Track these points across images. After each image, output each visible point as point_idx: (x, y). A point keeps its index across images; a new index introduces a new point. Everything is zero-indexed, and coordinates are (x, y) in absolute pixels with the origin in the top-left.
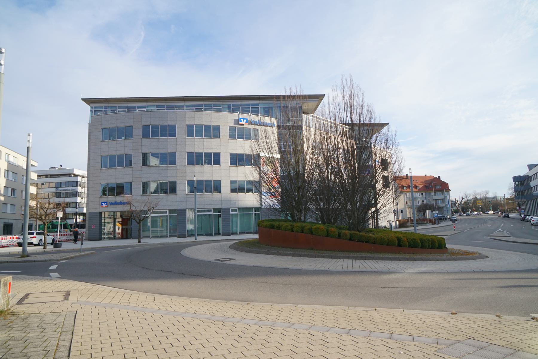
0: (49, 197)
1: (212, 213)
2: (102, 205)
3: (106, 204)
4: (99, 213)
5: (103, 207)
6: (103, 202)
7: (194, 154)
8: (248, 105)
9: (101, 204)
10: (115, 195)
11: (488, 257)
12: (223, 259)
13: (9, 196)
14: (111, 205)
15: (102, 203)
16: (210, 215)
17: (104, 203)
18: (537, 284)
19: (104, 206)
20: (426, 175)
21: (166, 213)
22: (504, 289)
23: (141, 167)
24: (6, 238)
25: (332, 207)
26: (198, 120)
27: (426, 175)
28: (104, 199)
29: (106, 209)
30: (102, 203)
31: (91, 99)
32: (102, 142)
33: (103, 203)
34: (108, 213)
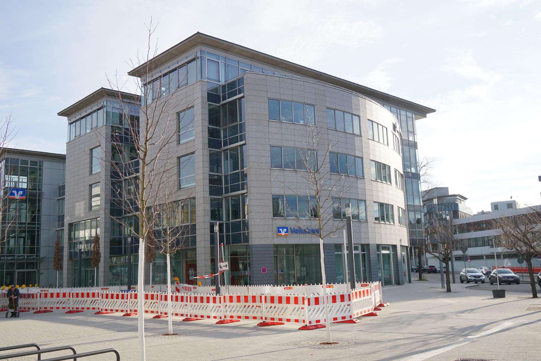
2: (280, 232)
3: (285, 230)
4: (272, 246)
5: (281, 235)
7: (296, 167)
9: (275, 229)
11: (466, 288)
12: (132, 338)
13: (93, 190)
14: (292, 232)
17: (283, 228)
18: (121, 360)
19: (283, 233)
21: (17, 256)
22: (487, 322)
24: (125, 297)
25: (126, 257)
28: (280, 222)
29: (285, 239)
30: (279, 228)
32: (270, 122)
33: (281, 230)
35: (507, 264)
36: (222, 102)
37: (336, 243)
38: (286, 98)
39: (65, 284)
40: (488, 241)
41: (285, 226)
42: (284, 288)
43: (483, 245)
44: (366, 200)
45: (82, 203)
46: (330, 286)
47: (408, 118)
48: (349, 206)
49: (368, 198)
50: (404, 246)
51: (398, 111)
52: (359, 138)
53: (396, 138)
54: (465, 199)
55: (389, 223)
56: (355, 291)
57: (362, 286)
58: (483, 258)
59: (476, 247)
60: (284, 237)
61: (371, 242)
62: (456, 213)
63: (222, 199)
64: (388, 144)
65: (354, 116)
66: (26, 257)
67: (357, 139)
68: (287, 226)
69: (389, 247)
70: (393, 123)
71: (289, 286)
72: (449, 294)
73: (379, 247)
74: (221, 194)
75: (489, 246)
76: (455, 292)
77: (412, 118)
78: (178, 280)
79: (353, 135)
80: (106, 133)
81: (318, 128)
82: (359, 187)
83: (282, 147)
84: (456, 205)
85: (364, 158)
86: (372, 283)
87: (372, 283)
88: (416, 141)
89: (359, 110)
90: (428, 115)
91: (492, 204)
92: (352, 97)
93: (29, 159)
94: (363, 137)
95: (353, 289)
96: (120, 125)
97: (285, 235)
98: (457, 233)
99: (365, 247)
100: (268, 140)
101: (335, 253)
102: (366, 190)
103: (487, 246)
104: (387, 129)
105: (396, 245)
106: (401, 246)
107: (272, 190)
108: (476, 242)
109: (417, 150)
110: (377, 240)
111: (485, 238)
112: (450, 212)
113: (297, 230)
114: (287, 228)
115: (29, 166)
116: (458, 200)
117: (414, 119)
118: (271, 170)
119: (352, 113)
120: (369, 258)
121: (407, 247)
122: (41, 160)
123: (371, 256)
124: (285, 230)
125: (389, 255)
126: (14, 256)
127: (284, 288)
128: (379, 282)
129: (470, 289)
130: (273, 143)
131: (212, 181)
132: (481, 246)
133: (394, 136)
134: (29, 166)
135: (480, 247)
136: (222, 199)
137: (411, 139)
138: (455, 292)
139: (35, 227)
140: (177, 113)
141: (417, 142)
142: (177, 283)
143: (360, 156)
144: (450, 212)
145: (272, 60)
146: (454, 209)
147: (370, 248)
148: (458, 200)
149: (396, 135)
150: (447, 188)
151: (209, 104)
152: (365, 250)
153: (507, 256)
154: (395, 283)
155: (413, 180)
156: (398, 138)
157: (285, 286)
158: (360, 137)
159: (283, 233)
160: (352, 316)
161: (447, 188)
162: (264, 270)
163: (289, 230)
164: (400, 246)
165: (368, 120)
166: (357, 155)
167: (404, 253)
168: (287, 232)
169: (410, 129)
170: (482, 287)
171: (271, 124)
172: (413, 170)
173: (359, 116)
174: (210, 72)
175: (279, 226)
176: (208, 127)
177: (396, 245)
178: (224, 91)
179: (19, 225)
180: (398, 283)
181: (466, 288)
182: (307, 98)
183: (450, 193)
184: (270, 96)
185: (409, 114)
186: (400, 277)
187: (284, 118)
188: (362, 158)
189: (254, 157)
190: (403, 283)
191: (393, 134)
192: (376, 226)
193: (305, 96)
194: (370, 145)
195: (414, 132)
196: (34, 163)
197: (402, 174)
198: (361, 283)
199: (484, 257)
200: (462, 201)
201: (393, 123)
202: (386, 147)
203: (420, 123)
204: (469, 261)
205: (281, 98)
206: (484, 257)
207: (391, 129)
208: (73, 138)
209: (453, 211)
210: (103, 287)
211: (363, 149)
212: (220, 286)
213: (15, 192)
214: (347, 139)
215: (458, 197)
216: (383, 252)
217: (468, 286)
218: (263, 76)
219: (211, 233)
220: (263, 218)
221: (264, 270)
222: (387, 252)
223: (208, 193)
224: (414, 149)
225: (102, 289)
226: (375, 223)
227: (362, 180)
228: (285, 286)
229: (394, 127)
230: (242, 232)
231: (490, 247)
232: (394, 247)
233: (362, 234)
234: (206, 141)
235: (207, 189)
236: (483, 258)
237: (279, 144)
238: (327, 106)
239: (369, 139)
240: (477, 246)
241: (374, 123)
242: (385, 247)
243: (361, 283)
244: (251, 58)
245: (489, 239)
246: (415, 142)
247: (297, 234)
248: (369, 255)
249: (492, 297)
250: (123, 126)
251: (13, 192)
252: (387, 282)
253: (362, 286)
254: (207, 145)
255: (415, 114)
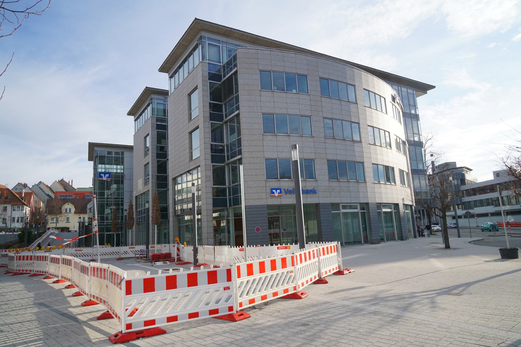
0: (2, 4)
1: (358, 210)
2: (274, 193)
3: (279, 191)
6: (274, 189)
8: (136, 211)
9: (269, 191)
10: (277, 178)
11: (469, 242)
15: (272, 189)
16: (364, 212)
17: (276, 190)
19: (276, 194)
20: (33, 186)
23: (324, 139)
26: (230, 165)
27: (33, 186)
28: (274, 183)
29: (279, 200)
30: (272, 189)
31: (216, 26)
34: (451, 239)
35: (510, 219)
36: (223, 79)
37: (333, 202)
38: (277, 69)
39: (134, 243)
40: (492, 202)
41: (279, 188)
42: (240, 249)
43: (488, 205)
44: (364, 162)
45: (141, 180)
46: (286, 247)
47: (409, 94)
48: (296, 148)
49: (365, 160)
50: (408, 205)
51: (399, 88)
52: (354, 105)
53: (397, 109)
54: (471, 170)
55: (390, 184)
56: (304, 252)
57: (240, 251)
58: (488, 216)
59: (481, 207)
60: (277, 197)
61: (370, 201)
62: (463, 180)
63: (225, 166)
64: (386, 113)
65: (348, 86)
66: (120, 223)
67: (352, 106)
68: (281, 187)
69: (391, 206)
70: (392, 95)
71: (280, 245)
72: (448, 251)
73: (380, 205)
74: (223, 161)
75: (493, 205)
76: (455, 249)
77: (413, 94)
78: (178, 240)
79: (348, 103)
80: (151, 123)
81: (311, 96)
82: (356, 150)
83: (274, 114)
84: (463, 175)
85: (360, 124)
86: (256, 247)
87: (256, 247)
88: (417, 113)
89: (354, 80)
90: (428, 92)
91: (494, 172)
92: (346, 68)
93: (113, 150)
94: (359, 105)
95: (302, 249)
96: (164, 116)
97: (278, 196)
98: (465, 196)
99: (365, 206)
100: (260, 108)
101: (332, 212)
102: (364, 153)
103: (490, 198)
104: (385, 99)
105: (398, 204)
106: (404, 204)
107: (265, 154)
108: (482, 203)
109: (419, 122)
110: (377, 199)
111: (489, 200)
112: (458, 180)
113: (290, 190)
114: (280, 189)
115: (113, 155)
116: (464, 171)
117: (415, 95)
118: (264, 136)
119: (346, 82)
120: (369, 215)
121: (411, 206)
122: (122, 150)
123: (371, 214)
124: (279, 191)
125: (391, 212)
126: (104, 222)
127: (240, 249)
128: (338, 243)
129: (474, 244)
130: (265, 110)
131: (214, 149)
132: (486, 206)
133: (394, 107)
134: (113, 155)
135: (485, 207)
136: (225, 166)
137: (413, 112)
138: (455, 249)
139: (119, 201)
140: (188, 95)
141: (418, 115)
142: (178, 243)
143: (356, 121)
144: (458, 180)
145: (272, 43)
146: (461, 178)
147: (370, 206)
148: (464, 171)
149: (395, 106)
150: (455, 162)
151: (210, 82)
152: (365, 209)
153: (510, 213)
154: (398, 238)
155: (416, 147)
156: (398, 109)
157: (279, 246)
158: (356, 105)
159: (276, 194)
160: (297, 288)
161: (455, 162)
162: (258, 230)
163: (283, 191)
164: (402, 205)
165: (364, 89)
166: (353, 121)
167: (408, 211)
168: (280, 193)
169: (412, 103)
170: (487, 241)
171: (263, 93)
172: (416, 139)
173: (354, 86)
174: (211, 53)
175: (273, 188)
176: (210, 103)
177: (398, 204)
178: (224, 70)
179: (114, 200)
180: (402, 238)
181: (469, 242)
182: (299, 69)
183: (458, 166)
184: (261, 68)
185: (410, 91)
186: (403, 233)
187: (276, 88)
188: (359, 123)
189: (246, 124)
190: (407, 238)
191: (393, 104)
192: (375, 186)
193: (297, 67)
194: (367, 112)
195: (415, 106)
196: (117, 153)
197: (403, 141)
198: (239, 247)
199: (489, 215)
200: (468, 172)
201: (392, 95)
202: (385, 115)
203: (422, 100)
204: (476, 218)
205: (273, 70)
206: (489, 215)
207: (389, 99)
208: (137, 131)
209: (460, 179)
210: (130, 247)
211: (360, 116)
212: (197, 246)
213: (103, 175)
214: (342, 106)
215: (464, 169)
216: (384, 210)
217: (472, 240)
218: (254, 50)
219: (213, 197)
220: (256, 180)
221: (258, 230)
222: (389, 210)
223: (210, 161)
224: (416, 120)
225: (129, 248)
226: (374, 183)
227: (359, 144)
228: (279, 246)
229: (394, 99)
230: (239, 195)
231: (494, 206)
232: (397, 205)
233: (360, 193)
234: (208, 115)
235: (209, 157)
236: (488, 216)
237: (271, 111)
238: (320, 76)
239: (365, 106)
240: (482, 206)
241: (370, 92)
242: (387, 205)
243: (239, 247)
244: (252, 43)
245: (493, 200)
246: (416, 114)
247: (291, 195)
248: (369, 213)
249: (499, 256)
250: (167, 117)
251: (101, 175)
252: (346, 243)
253: (240, 251)
254: (209, 119)
255: (416, 91)
